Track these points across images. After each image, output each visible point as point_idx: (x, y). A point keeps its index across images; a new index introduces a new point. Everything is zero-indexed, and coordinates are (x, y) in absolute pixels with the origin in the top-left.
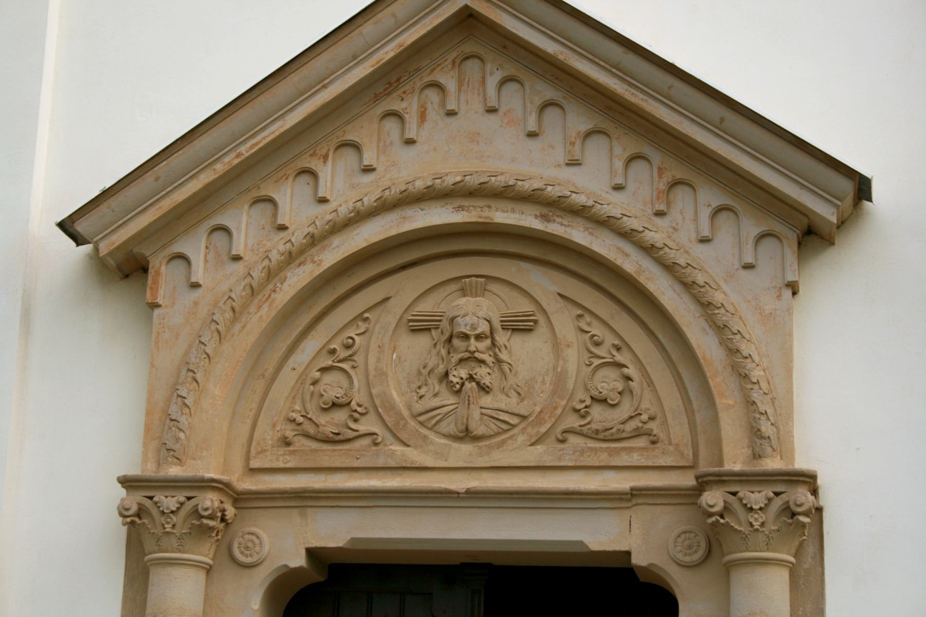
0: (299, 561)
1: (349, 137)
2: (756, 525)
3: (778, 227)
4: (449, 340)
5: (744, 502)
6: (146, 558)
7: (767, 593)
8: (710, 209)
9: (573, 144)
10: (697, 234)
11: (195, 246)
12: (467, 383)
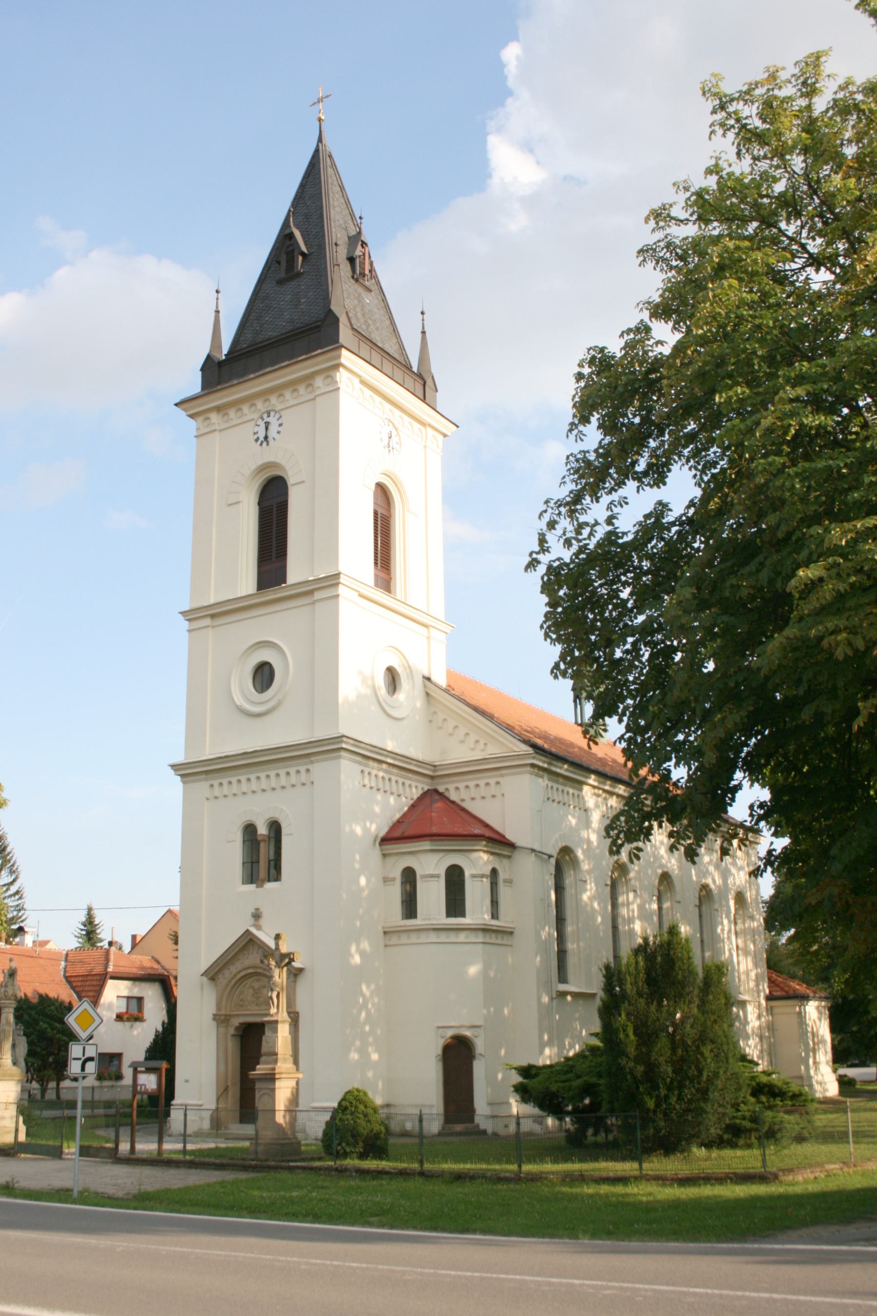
11: (220, 976)
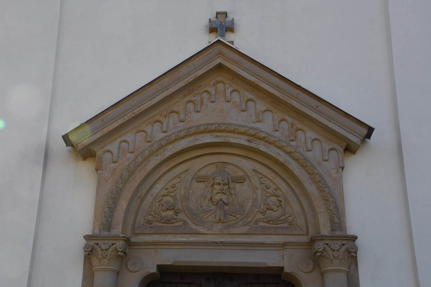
0: (154, 270)
1: (175, 109)
2: (336, 256)
3: (336, 147)
4: (213, 185)
5: (331, 247)
6: (93, 269)
7: (335, 285)
8: (311, 139)
9: (259, 115)
10: (312, 146)
12: (219, 202)
